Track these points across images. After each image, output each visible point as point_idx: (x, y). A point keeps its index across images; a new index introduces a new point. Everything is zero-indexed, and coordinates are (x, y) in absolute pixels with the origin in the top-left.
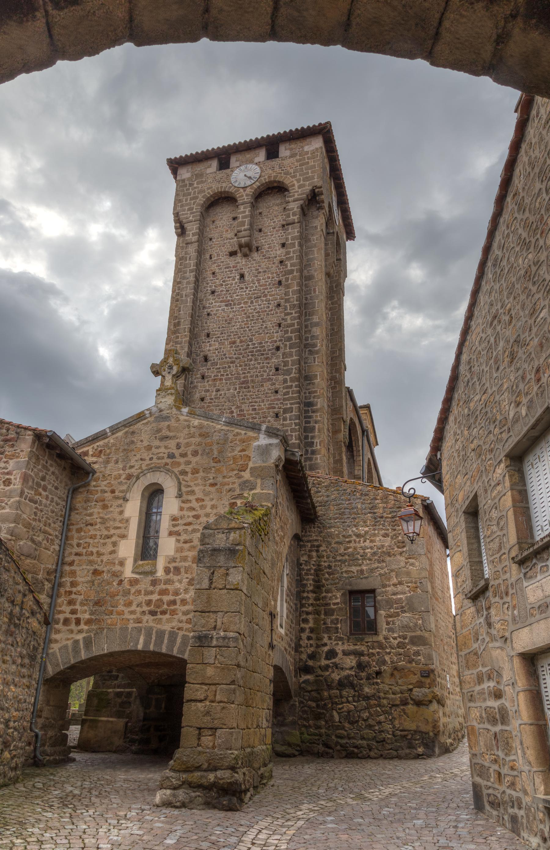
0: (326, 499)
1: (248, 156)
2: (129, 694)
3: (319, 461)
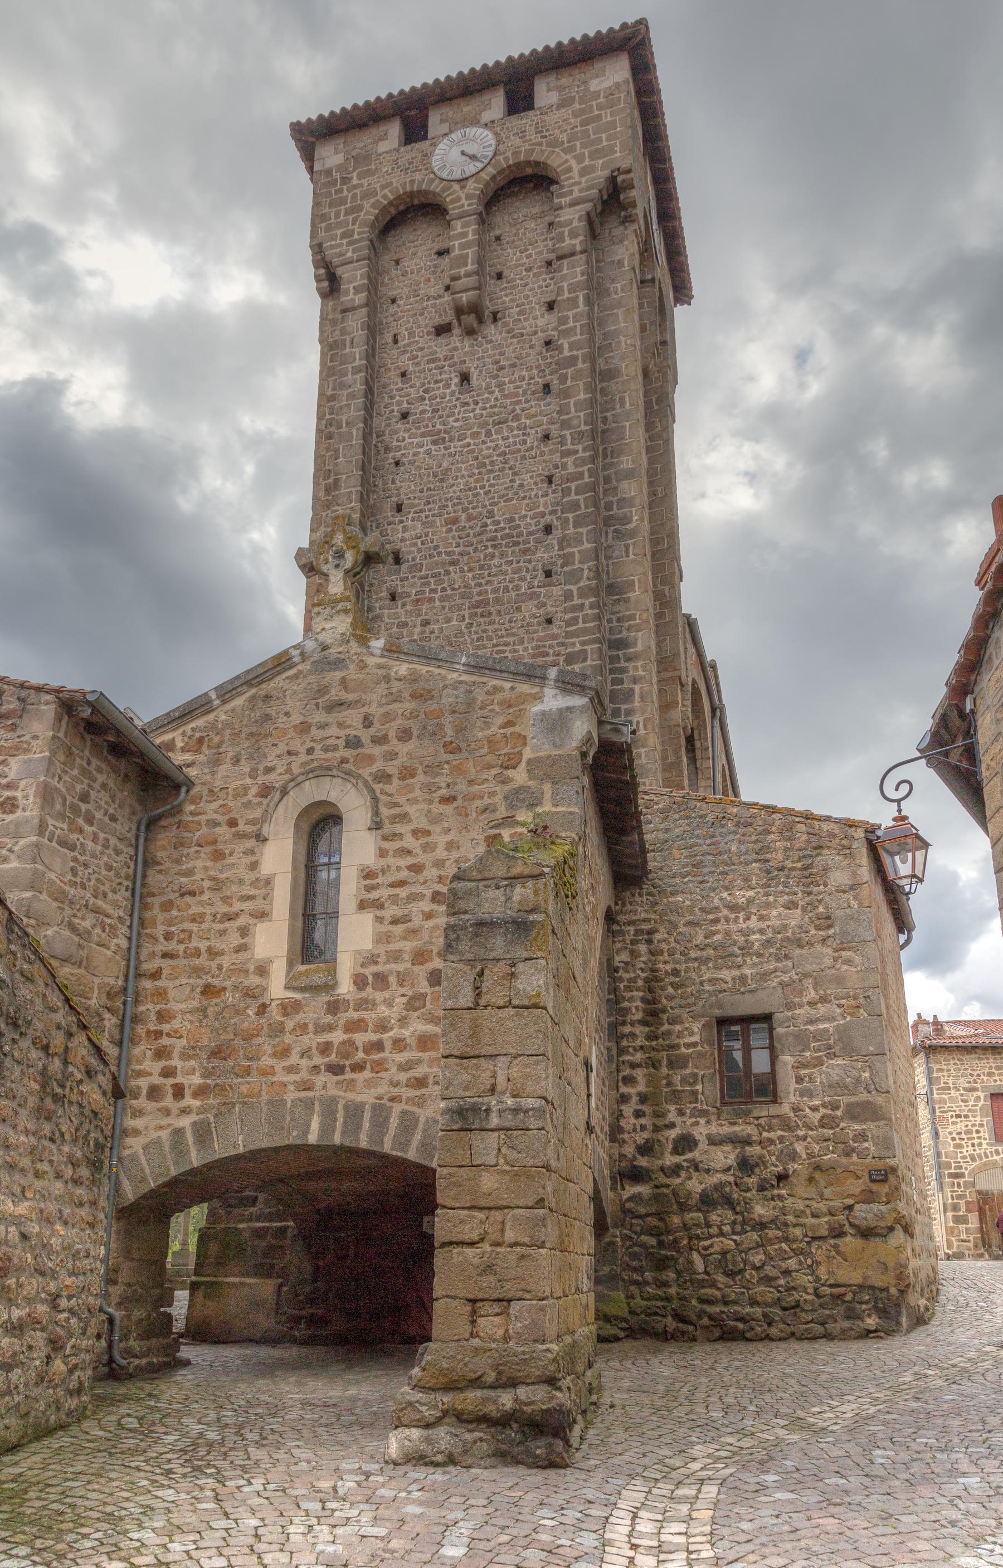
0: (662, 836)
1: (467, 108)
2: (282, 1231)
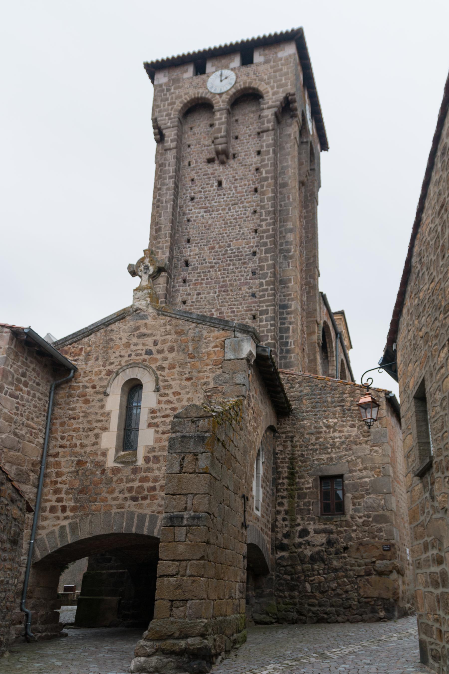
3: (293, 359)
